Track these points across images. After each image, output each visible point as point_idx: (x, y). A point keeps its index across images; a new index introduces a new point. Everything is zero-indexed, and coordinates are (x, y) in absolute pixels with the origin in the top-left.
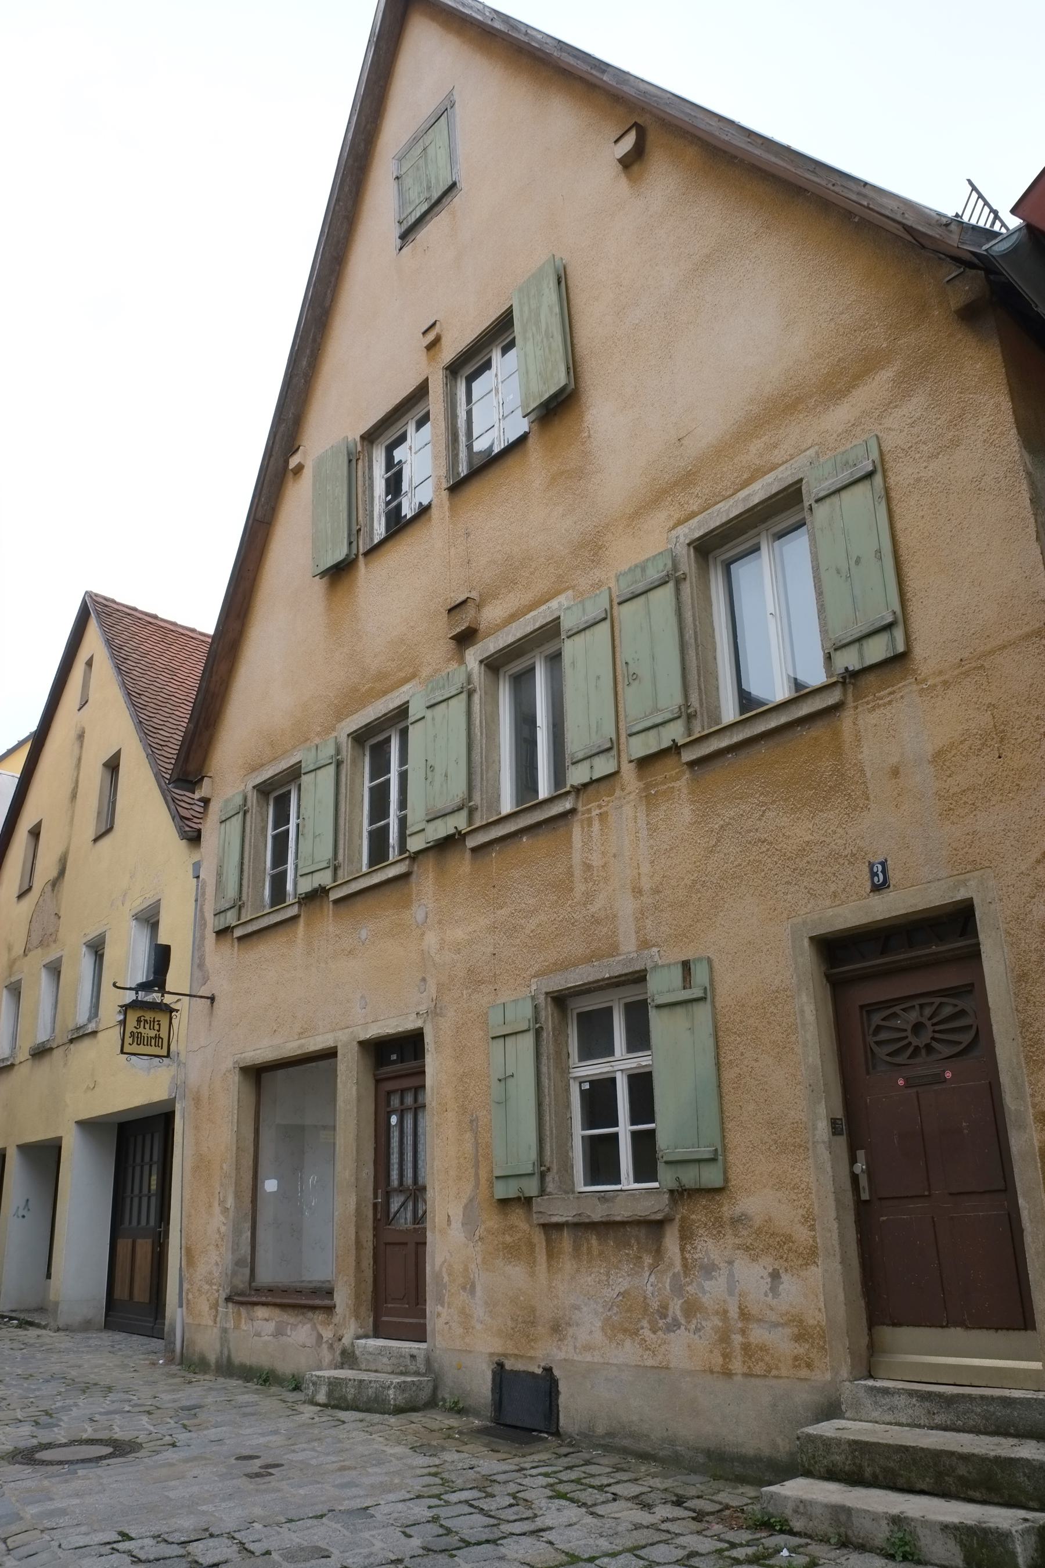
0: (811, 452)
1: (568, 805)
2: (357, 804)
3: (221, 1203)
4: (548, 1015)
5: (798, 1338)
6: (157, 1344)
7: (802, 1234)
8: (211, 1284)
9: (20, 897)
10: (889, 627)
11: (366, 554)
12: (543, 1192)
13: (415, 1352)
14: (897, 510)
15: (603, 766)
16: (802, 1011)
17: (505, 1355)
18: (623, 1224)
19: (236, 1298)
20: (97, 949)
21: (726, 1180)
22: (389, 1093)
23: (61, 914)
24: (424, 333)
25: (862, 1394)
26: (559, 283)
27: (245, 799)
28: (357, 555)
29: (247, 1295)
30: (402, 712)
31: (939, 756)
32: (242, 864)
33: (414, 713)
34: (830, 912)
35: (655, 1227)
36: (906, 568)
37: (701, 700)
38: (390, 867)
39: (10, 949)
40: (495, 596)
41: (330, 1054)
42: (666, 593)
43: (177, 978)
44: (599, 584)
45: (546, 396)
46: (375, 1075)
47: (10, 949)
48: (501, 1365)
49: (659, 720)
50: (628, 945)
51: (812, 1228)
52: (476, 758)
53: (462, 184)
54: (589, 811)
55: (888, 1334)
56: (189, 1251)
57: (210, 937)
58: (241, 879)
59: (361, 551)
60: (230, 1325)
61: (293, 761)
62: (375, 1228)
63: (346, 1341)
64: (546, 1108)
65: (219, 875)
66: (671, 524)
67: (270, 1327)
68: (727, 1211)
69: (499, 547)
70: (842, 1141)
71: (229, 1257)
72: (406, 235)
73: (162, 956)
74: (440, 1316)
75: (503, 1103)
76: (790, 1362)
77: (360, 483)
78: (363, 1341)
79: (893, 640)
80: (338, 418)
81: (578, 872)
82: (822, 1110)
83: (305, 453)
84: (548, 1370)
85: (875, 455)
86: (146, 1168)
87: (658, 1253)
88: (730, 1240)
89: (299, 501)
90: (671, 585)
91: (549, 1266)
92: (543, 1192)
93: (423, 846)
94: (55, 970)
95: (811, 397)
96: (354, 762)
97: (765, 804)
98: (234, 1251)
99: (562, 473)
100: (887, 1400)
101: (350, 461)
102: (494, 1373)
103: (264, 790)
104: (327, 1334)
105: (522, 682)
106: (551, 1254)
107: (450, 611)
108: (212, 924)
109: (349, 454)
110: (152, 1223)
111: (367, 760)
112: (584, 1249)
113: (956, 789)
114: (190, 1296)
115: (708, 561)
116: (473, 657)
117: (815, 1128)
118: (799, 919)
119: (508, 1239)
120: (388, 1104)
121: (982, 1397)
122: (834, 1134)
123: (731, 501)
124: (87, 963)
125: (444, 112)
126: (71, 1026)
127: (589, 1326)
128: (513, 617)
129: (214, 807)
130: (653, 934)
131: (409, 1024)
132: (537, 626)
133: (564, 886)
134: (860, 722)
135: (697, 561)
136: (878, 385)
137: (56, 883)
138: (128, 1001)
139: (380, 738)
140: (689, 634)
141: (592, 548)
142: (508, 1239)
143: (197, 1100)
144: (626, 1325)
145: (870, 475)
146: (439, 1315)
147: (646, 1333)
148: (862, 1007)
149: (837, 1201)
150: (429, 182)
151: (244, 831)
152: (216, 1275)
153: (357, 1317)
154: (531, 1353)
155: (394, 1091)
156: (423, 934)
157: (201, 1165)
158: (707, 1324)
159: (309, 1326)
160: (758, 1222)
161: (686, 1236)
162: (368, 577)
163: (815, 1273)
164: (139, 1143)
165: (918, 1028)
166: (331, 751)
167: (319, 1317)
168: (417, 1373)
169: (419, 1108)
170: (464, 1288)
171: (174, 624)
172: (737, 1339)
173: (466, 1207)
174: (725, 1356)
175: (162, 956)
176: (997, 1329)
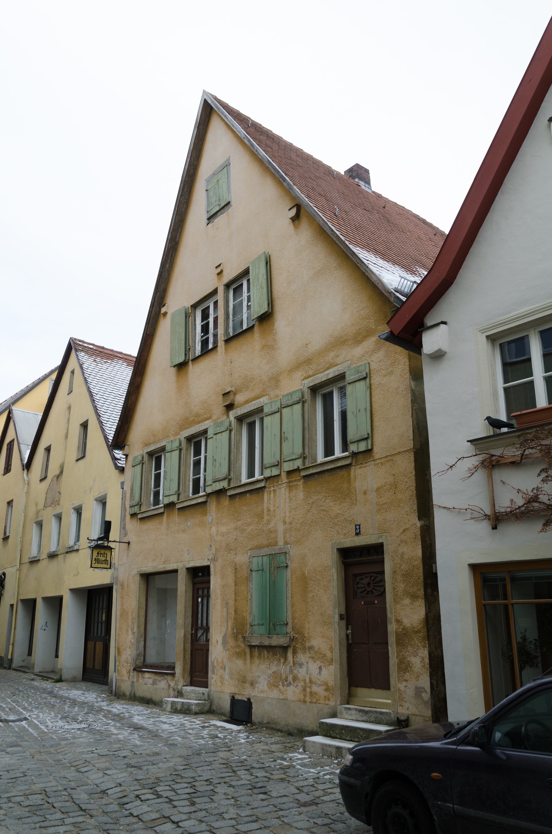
0: (349, 362)
1: (263, 484)
3: (132, 630)
5: (326, 690)
6: (105, 687)
7: (329, 654)
8: (128, 663)
9: (41, 480)
10: (366, 439)
11: (192, 360)
13: (204, 692)
14: (373, 394)
16: (333, 575)
17: (235, 694)
18: (275, 647)
20: (79, 511)
22: (198, 589)
24: (216, 267)
25: (343, 710)
26: (267, 264)
27: (143, 458)
28: (189, 360)
29: (141, 667)
30: (205, 432)
31: (378, 489)
33: (210, 434)
34: (343, 540)
36: (374, 417)
37: (309, 451)
38: (197, 501)
39: (37, 505)
40: (241, 391)
41: (176, 571)
42: (298, 407)
43: (114, 535)
44: (277, 396)
45: (260, 314)
46: (193, 581)
47: (37, 505)
48: (233, 697)
49: (294, 458)
50: (281, 543)
51: (332, 652)
52: (232, 458)
53: (232, 203)
54: (270, 487)
55: (353, 689)
56: (118, 649)
57: (128, 517)
58: (141, 493)
60: (135, 680)
61: (162, 444)
62: (192, 643)
65: (132, 490)
66: (302, 378)
67: (151, 681)
69: (243, 371)
70: (344, 622)
71: (135, 653)
72: (210, 219)
73: (107, 526)
74: (213, 678)
76: (323, 698)
77: (190, 327)
78: (185, 687)
79: (368, 443)
80: (179, 299)
81: (265, 511)
82: (337, 610)
84: (249, 699)
85: (367, 371)
86: (101, 610)
87: (286, 658)
89: (165, 328)
91: (251, 661)
93: (211, 491)
94: (59, 517)
95: (350, 340)
96: (187, 449)
97: (325, 496)
98: (137, 650)
99: (266, 346)
100: (350, 712)
101: (186, 317)
102: (231, 700)
103: (151, 454)
105: (251, 426)
106: (252, 657)
107: (224, 395)
108: (129, 511)
109: (186, 313)
110: (103, 635)
112: (262, 655)
113: (381, 503)
114: (119, 668)
115: (316, 396)
116: (232, 414)
117: (334, 617)
118: (334, 541)
119: (237, 650)
120: (198, 593)
121: (375, 712)
122: (341, 619)
123: (323, 374)
124: (74, 517)
125: (227, 165)
126: (67, 546)
127: (263, 684)
128: (247, 402)
130: (289, 540)
131: (205, 563)
132: (255, 408)
133: (260, 516)
134: (356, 472)
135: (311, 395)
136: (370, 342)
137: (59, 476)
139: (198, 439)
140: (306, 424)
142: (237, 650)
143: (122, 586)
144: (275, 684)
145: (365, 378)
146: (213, 678)
147: (281, 686)
148: (353, 575)
149: (340, 643)
150: (219, 197)
151: (142, 472)
152: (130, 659)
153: (184, 678)
154: (244, 693)
155: (200, 588)
156: (211, 527)
157: (124, 614)
159: (165, 681)
160: (316, 649)
161: (295, 653)
162: (192, 368)
163: (332, 667)
164: (97, 601)
165: (369, 584)
166: (177, 444)
167: (169, 678)
168: (205, 700)
169: (208, 596)
170: (222, 668)
172: (308, 690)
173: (223, 637)
174: (305, 696)
175: (107, 526)
176: (384, 689)
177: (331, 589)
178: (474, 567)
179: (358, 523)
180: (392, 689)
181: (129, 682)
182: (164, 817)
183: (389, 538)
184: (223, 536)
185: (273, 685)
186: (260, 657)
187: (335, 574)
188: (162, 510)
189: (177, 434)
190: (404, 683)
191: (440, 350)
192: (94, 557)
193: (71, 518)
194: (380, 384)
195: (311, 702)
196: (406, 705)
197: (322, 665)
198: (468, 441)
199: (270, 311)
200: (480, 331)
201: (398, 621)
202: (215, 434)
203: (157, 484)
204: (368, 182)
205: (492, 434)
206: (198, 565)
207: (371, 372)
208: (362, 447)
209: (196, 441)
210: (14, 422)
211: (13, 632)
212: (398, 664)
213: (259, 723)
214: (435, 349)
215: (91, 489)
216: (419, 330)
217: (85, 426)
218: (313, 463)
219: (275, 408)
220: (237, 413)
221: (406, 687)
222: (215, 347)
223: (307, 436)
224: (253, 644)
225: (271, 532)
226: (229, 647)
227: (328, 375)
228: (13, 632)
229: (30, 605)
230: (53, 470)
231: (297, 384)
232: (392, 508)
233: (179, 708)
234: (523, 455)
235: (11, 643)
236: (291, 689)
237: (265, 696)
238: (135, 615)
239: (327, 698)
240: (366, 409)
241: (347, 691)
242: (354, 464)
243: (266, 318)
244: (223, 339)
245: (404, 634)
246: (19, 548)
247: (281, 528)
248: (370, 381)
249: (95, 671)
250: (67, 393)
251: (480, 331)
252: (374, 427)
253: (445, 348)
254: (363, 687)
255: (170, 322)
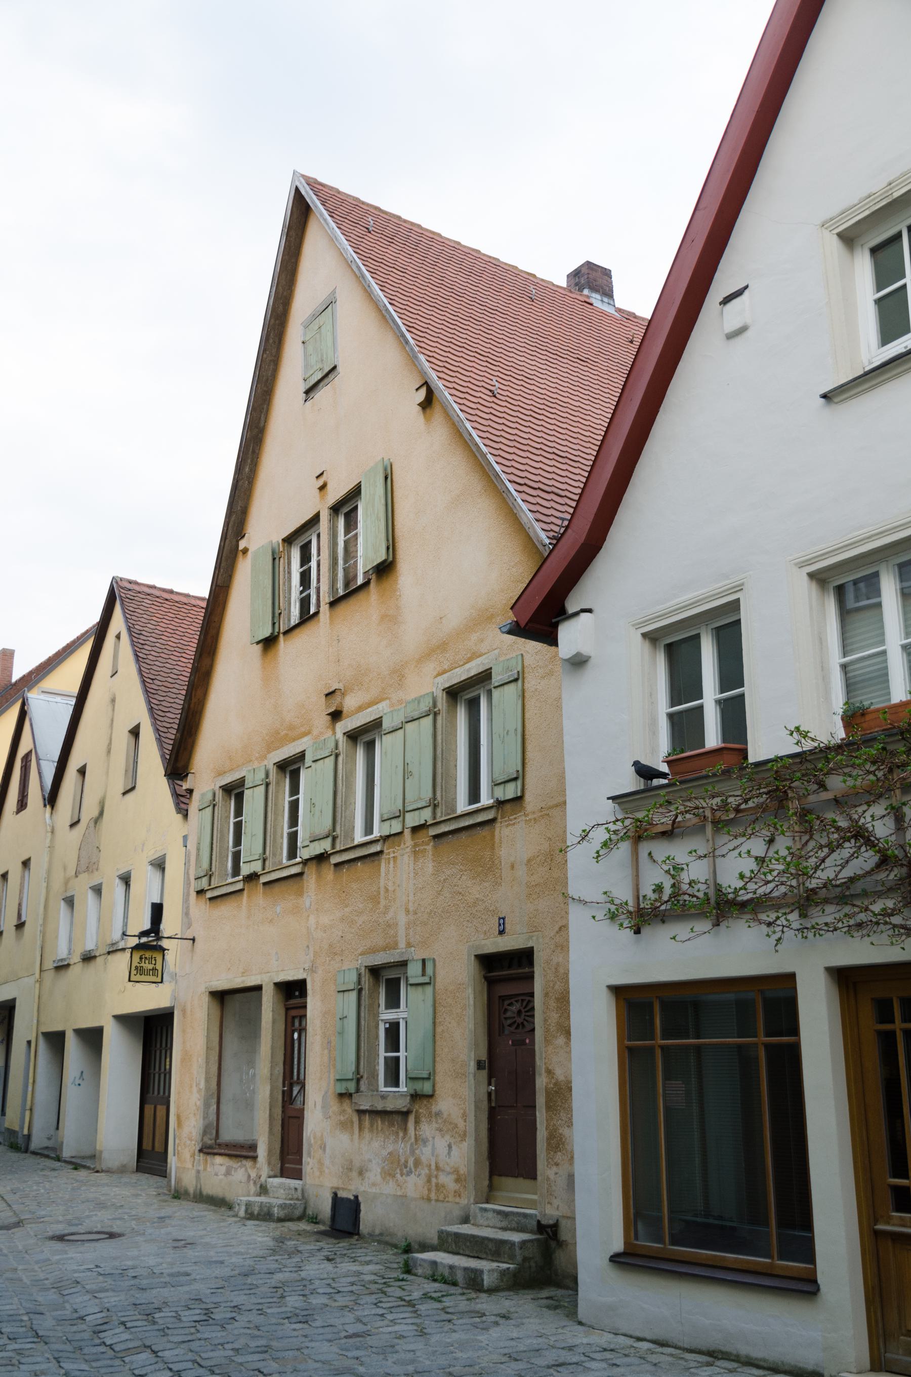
0: (496, 652)
2: (278, 813)
4: (366, 980)
5: (457, 1181)
7: (461, 1124)
8: (191, 1140)
9: (73, 825)
10: (515, 779)
11: (285, 633)
12: (358, 1090)
13: (297, 1186)
14: (527, 707)
15: (396, 827)
17: (338, 1188)
19: (205, 1150)
20: (126, 880)
21: (434, 1091)
22: (294, 1018)
23: (101, 848)
24: (317, 477)
25: (477, 1211)
26: (386, 478)
28: (279, 633)
30: (301, 756)
31: (529, 861)
32: (212, 844)
35: (405, 1114)
39: (65, 868)
41: (258, 988)
42: (427, 722)
43: (168, 926)
44: (400, 701)
45: (375, 564)
47: (65, 868)
48: (335, 1194)
50: (402, 945)
52: (339, 801)
55: (496, 1179)
58: (211, 855)
59: (282, 631)
60: (201, 1168)
62: (283, 1107)
63: (263, 1179)
64: (362, 1039)
65: (198, 849)
66: (435, 674)
67: (223, 1169)
68: (434, 1109)
70: (484, 1073)
73: (157, 911)
74: (309, 1164)
75: (341, 1033)
77: (281, 573)
80: (266, 529)
83: (249, 539)
84: (356, 1197)
85: (519, 669)
86: (163, 1052)
87: (405, 1130)
88: (435, 1125)
90: (431, 717)
92: (358, 1090)
94: (98, 890)
96: (278, 783)
97: (461, 870)
98: (204, 1118)
100: (485, 1214)
101: (274, 559)
104: (253, 1175)
106: (361, 1129)
107: (327, 695)
108: (194, 886)
109: (273, 553)
111: (288, 780)
112: (375, 1126)
113: (533, 883)
116: (344, 726)
118: (470, 944)
120: (293, 1024)
121: (517, 1213)
122: (478, 1069)
124: (120, 888)
125: (329, 304)
126: (109, 942)
128: (360, 709)
129: (196, 795)
133: (375, 899)
135: (448, 702)
137: (98, 819)
138: (133, 944)
139: (295, 767)
141: (398, 674)
142: (342, 1118)
145: (516, 680)
147: (398, 1176)
148: (500, 997)
149: (476, 1107)
150: (322, 356)
152: (194, 1134)
158: (423, 1172)
159: (243, 1169)
161: (417, 1122)
162: (284, 646)
165: (519, 1012)
166: (262, 775)
167: (248, 1163)
168: (297, 1199)
171: (187, 596)
172: (434, 1180)
177: (466, 1020)
178: (618, 991)
179: (503, 916)
180: (539, 1178)
181: (194, 1172)
182: (145, 1347)
183: (541, 940)
184: (325, 931)
185: (388, 1174)
186: (371, 1130)
187: (472, 996)
188: (240, 886)
189: (264, 757)
190: (555, 1169)
191: (578, 654)
192: (135, 964)
194: (536, 690)
195: (437, 1200)
196: (556, 1202)
197: (452, 1140)
198: (608, 798)
199: (391, 559)
200: (633, 625)
201: (549, 1072)
202: (314, 761)
203: (238, 841)
204: (608, 293)
205: (642, 787)
206: (291, 978)
207: (526, 670)
208: (510, 791)
209: (291, 768)
210: (30, 720)
211: (30, 1088)
212: (547, 1139)
213: (369, 1234)
215: (143, 845)
216: (554, 620)
218: (449, 814)
219: (396, 723)
220: (347, 727)
221: (556, 1174)
222: (317, 613)
223: (439, 771)
224: (362, 1108)
225: (389, 926)
226: (331, 1114)
227: (468, 670)
228: (30, 1088)
229: (56, 1040)
230: (89, 811)
231: (428, 684)
232: (547, 893)
233: (256, 1212)
234: (674, 821)
235: (28, 1107)
236: (412, 1179)
237: (378, 1191)
238: (201, 1060)
239: (457, 1194)
240: (516, 730)
241: (487, 1183)
242: (499, 820)
243: (384, 570)
244: (327, 601)
245: (556, 1092)
246: (39, 943)
247: (402, 919)
248: (523, 685)
249: (151, 1157)
250: (110, 674)
251: (633, 625)
252: (527, 761)
253: (586, 650)
254: (507, 1176)
255: (250, 566)
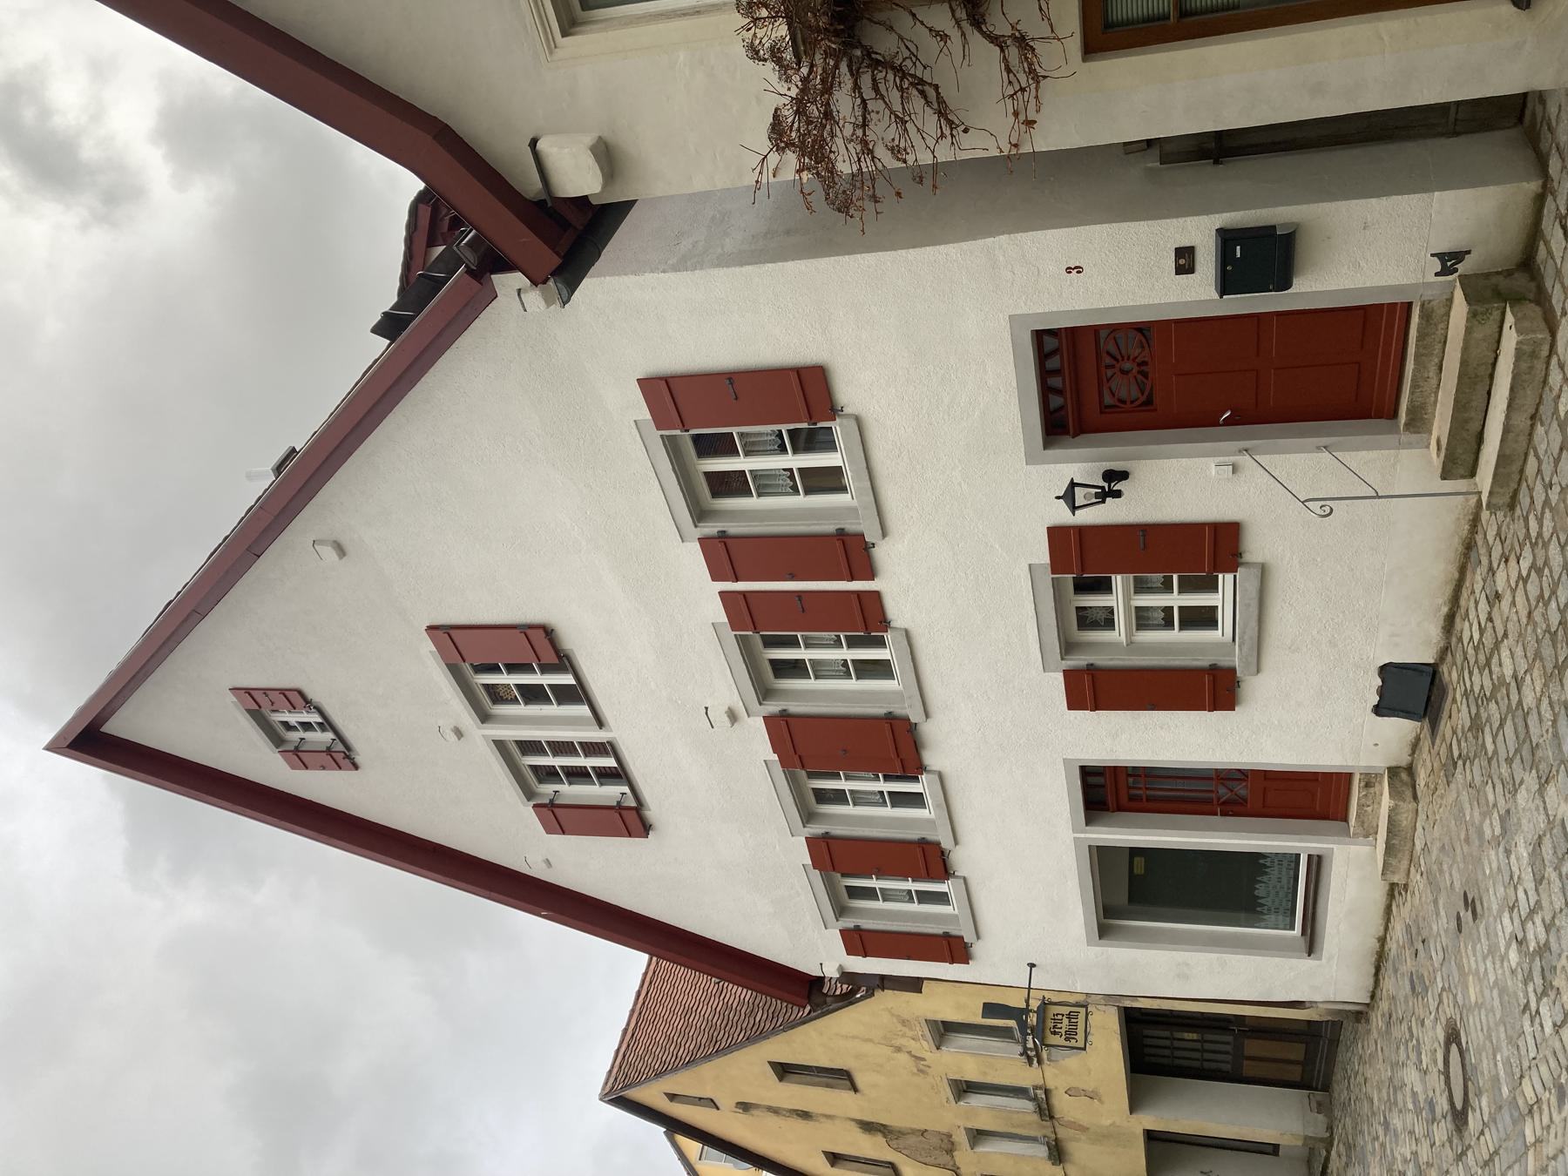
6: (1346, 1035)
20: (964, 1089)
86: (1176, 1044)
94: (978, 1136)
110: (1230, 1038)
124: (976, 1101)
193: (982, 1111)
200: (551, 53)
214: (589, 161)
217: (784, 1071)
251: (551, 53)
